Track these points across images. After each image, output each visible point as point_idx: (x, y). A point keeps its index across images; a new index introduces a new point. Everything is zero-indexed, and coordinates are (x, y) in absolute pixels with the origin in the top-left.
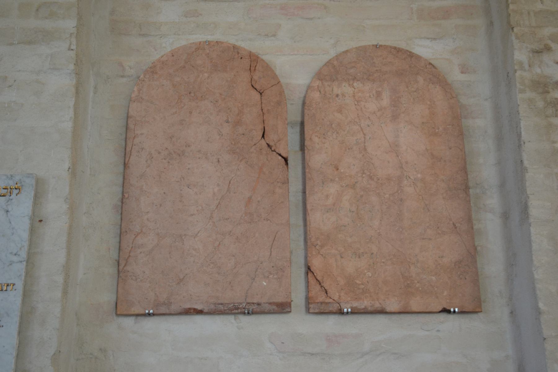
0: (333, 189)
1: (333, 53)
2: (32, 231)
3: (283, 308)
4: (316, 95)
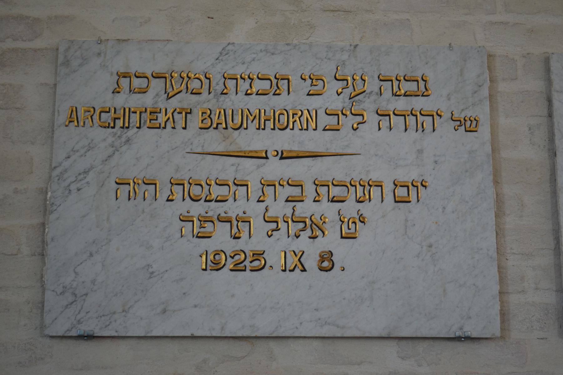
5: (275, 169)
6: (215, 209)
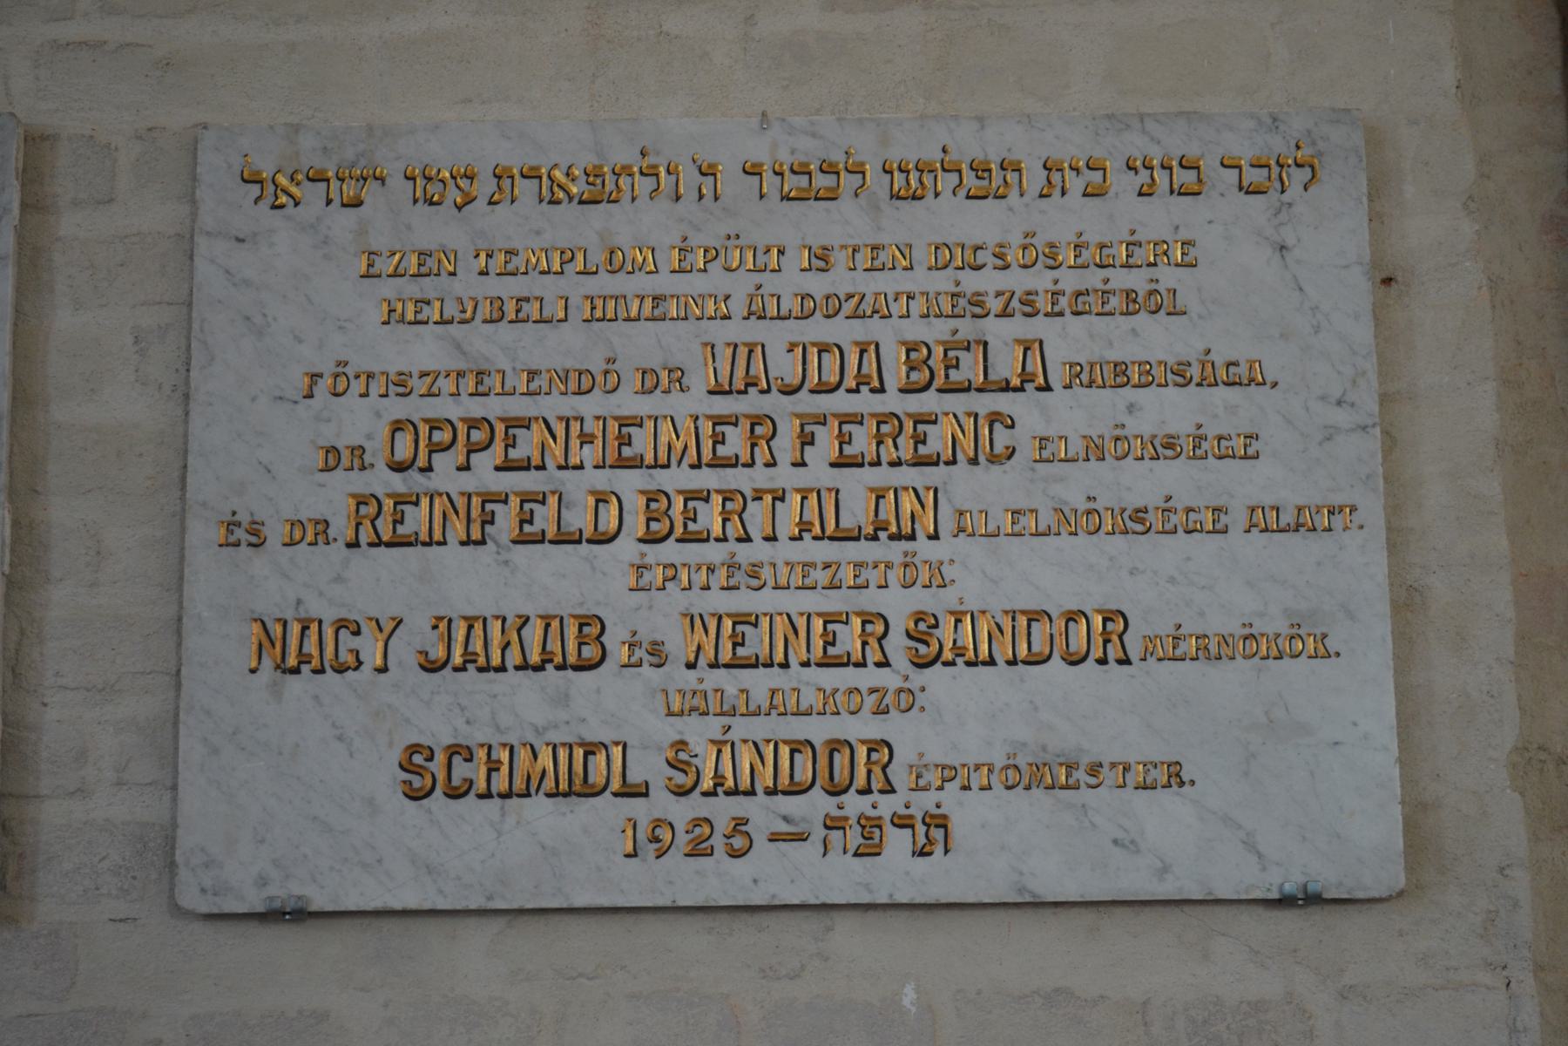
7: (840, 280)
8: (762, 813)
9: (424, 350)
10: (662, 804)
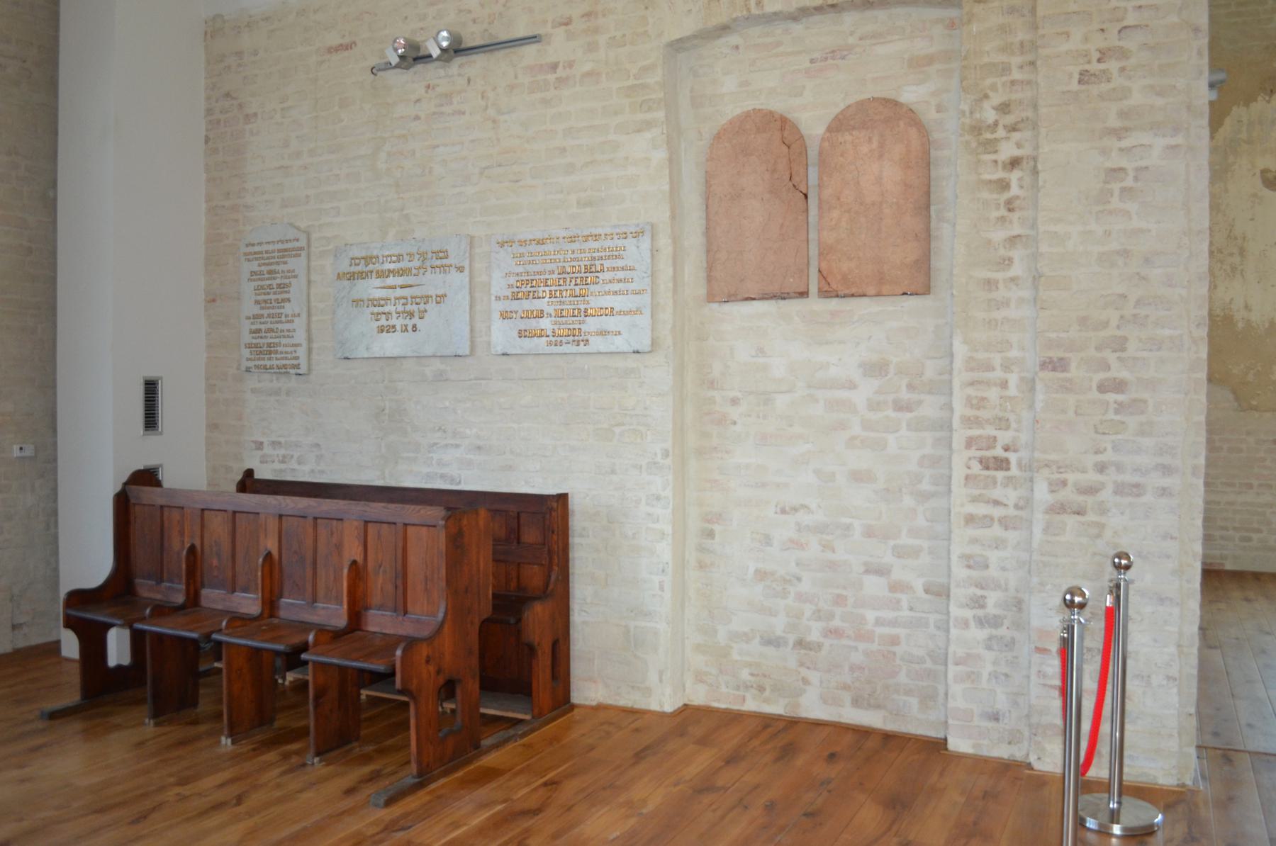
0: (835, 214)
1: (842, 106)
2: (653, 256)
3: (804, 294)
4: (826, 144)
5: (399, 292)
6: (381, 309)
7: (575, 256)
8: (564, 340)
9: (520, 269)
10: (551, 338)
